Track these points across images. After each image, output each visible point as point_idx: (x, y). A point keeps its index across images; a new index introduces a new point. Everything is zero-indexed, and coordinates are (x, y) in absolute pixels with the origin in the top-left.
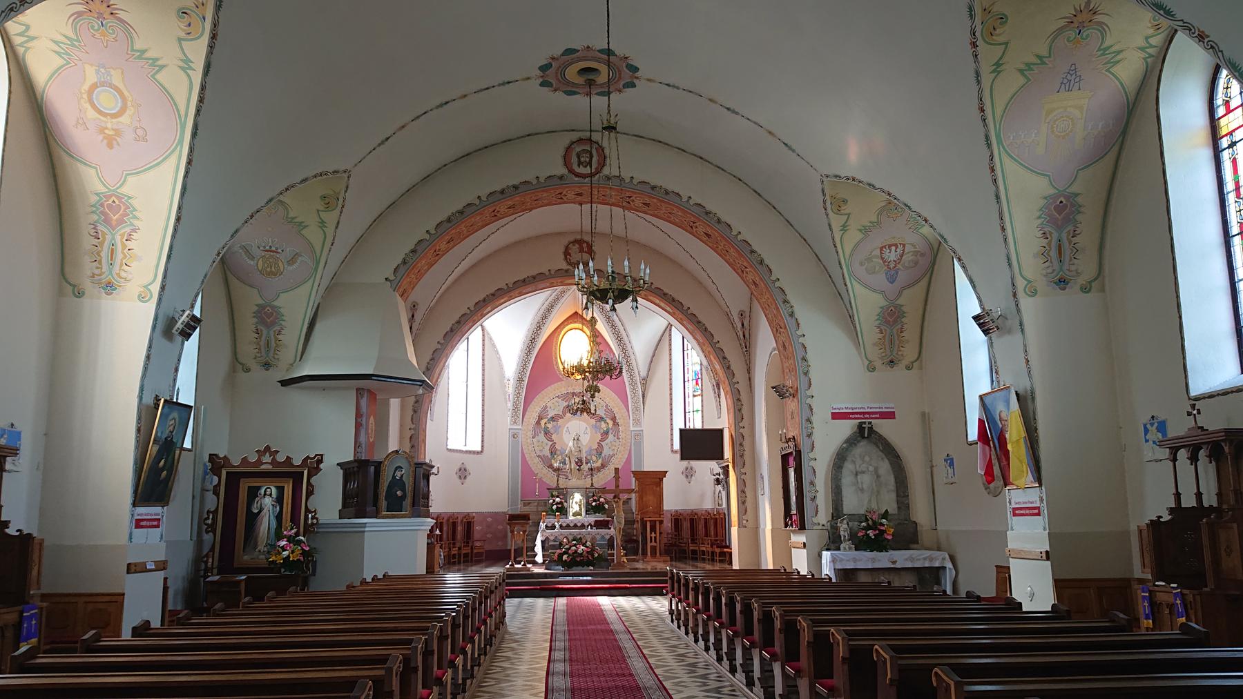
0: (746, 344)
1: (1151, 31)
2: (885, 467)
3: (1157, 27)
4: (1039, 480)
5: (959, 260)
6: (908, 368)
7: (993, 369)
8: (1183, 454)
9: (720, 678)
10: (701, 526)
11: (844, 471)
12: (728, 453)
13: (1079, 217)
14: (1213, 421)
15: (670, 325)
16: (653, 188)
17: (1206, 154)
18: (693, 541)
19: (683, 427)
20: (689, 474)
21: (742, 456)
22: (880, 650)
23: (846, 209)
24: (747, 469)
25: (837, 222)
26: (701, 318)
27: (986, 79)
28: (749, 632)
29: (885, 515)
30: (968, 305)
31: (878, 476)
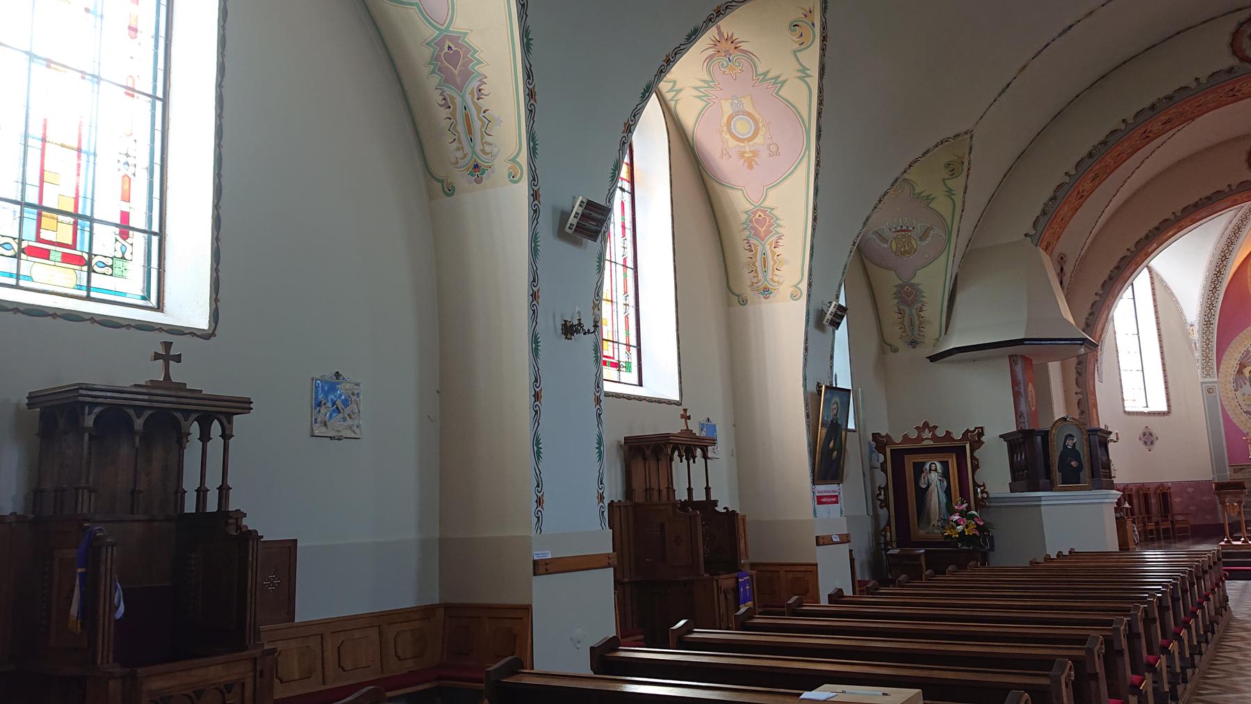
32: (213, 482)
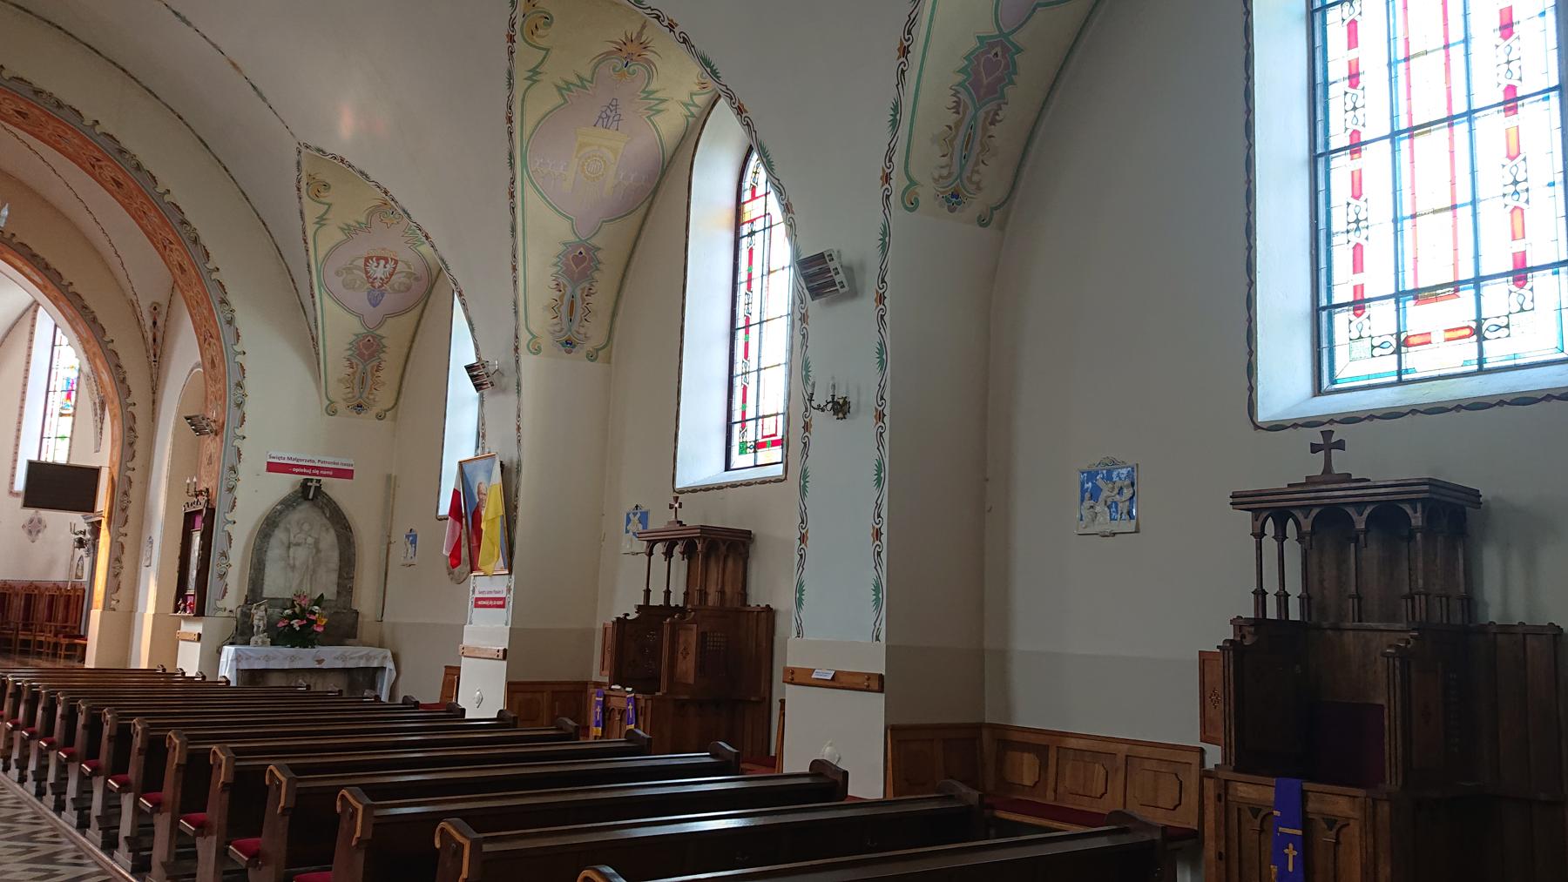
0: (157, 352)
1: (696, 88)
2: (329, 538)
3: (703, 86)
4: (510, 567)
5: (460, 295)
6: (379, 417)
7: (480, 435)
8: (659, 549)
9: (37, 819)
10: (42, 606)
11: (273, 542)
12: (102, 503)
13: (596, 275)
14: (694, 516)
15: (35, 305)
16: (38, 92)
17: (729, 237)
18: (26, 627)
19: (35, 458)
20: (34, 529)
21: (124, 510)
22: (277, 772)
23: (327, 197)
24: (129, 529)
25: (312, 210)
26: (89, 302)
27: (520, 84)
28: (92, 753)
29: (319, 601)
30: (463, 351)
31: (318, 551)
32: (1269, 543)
